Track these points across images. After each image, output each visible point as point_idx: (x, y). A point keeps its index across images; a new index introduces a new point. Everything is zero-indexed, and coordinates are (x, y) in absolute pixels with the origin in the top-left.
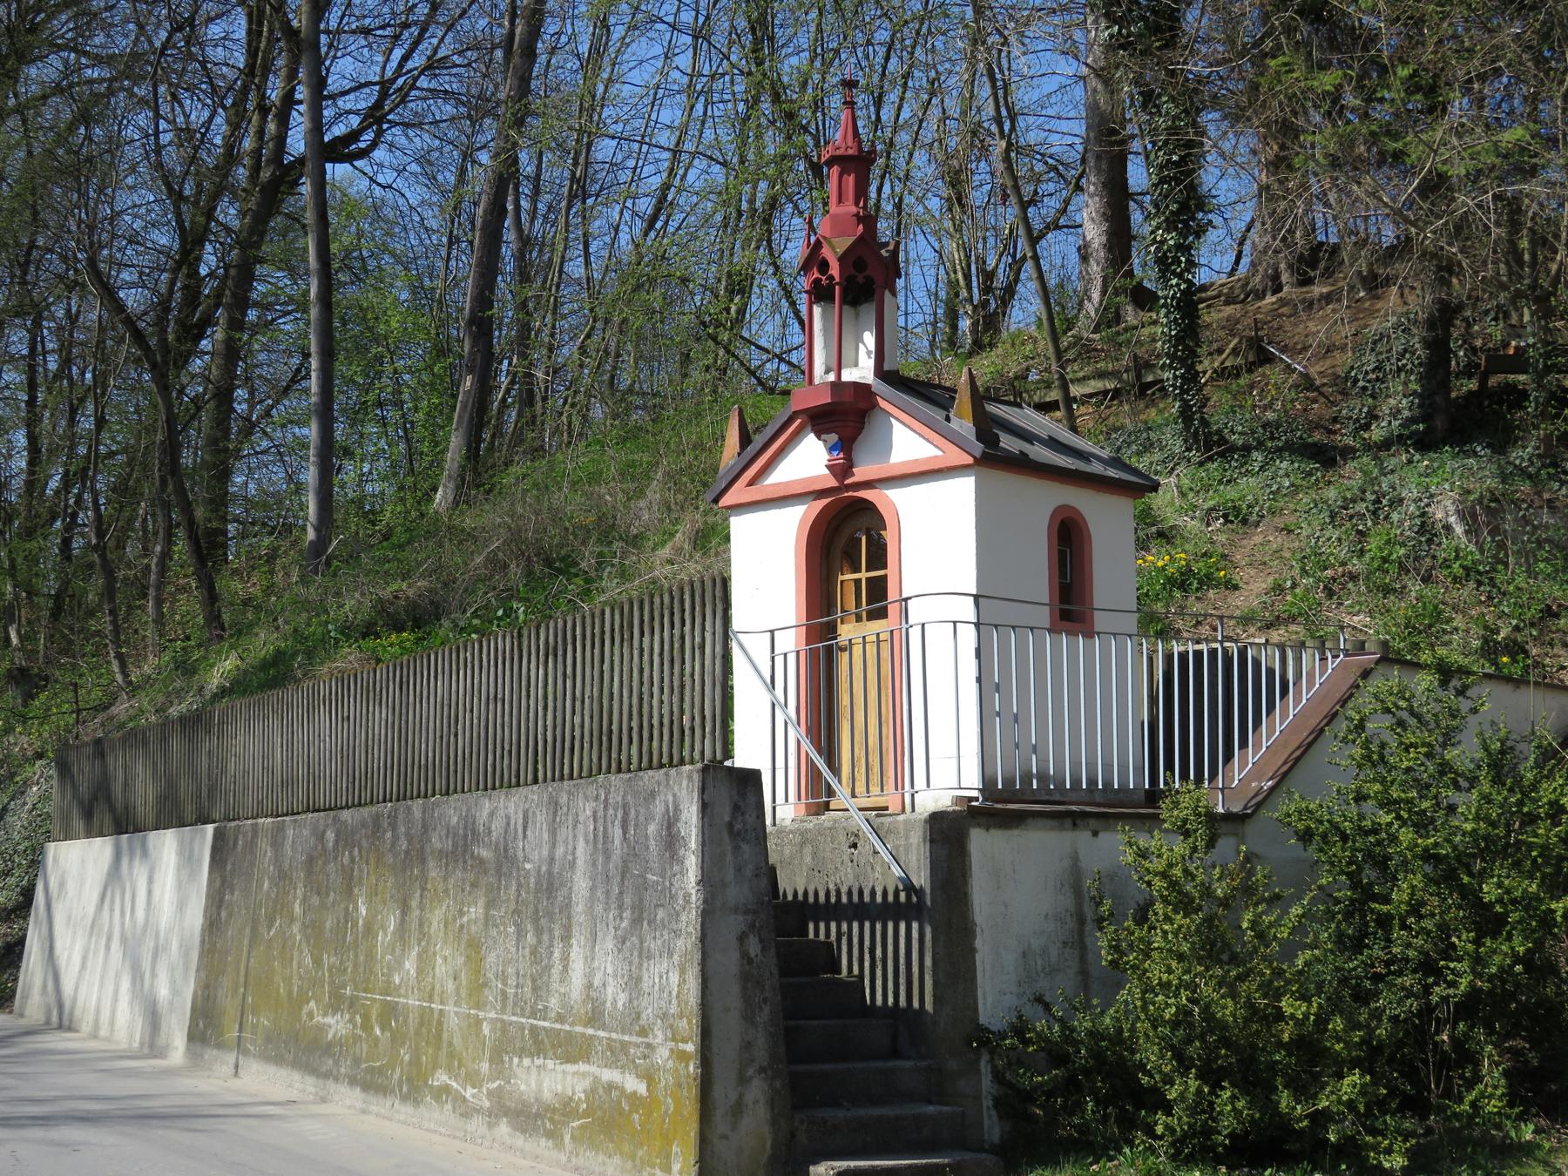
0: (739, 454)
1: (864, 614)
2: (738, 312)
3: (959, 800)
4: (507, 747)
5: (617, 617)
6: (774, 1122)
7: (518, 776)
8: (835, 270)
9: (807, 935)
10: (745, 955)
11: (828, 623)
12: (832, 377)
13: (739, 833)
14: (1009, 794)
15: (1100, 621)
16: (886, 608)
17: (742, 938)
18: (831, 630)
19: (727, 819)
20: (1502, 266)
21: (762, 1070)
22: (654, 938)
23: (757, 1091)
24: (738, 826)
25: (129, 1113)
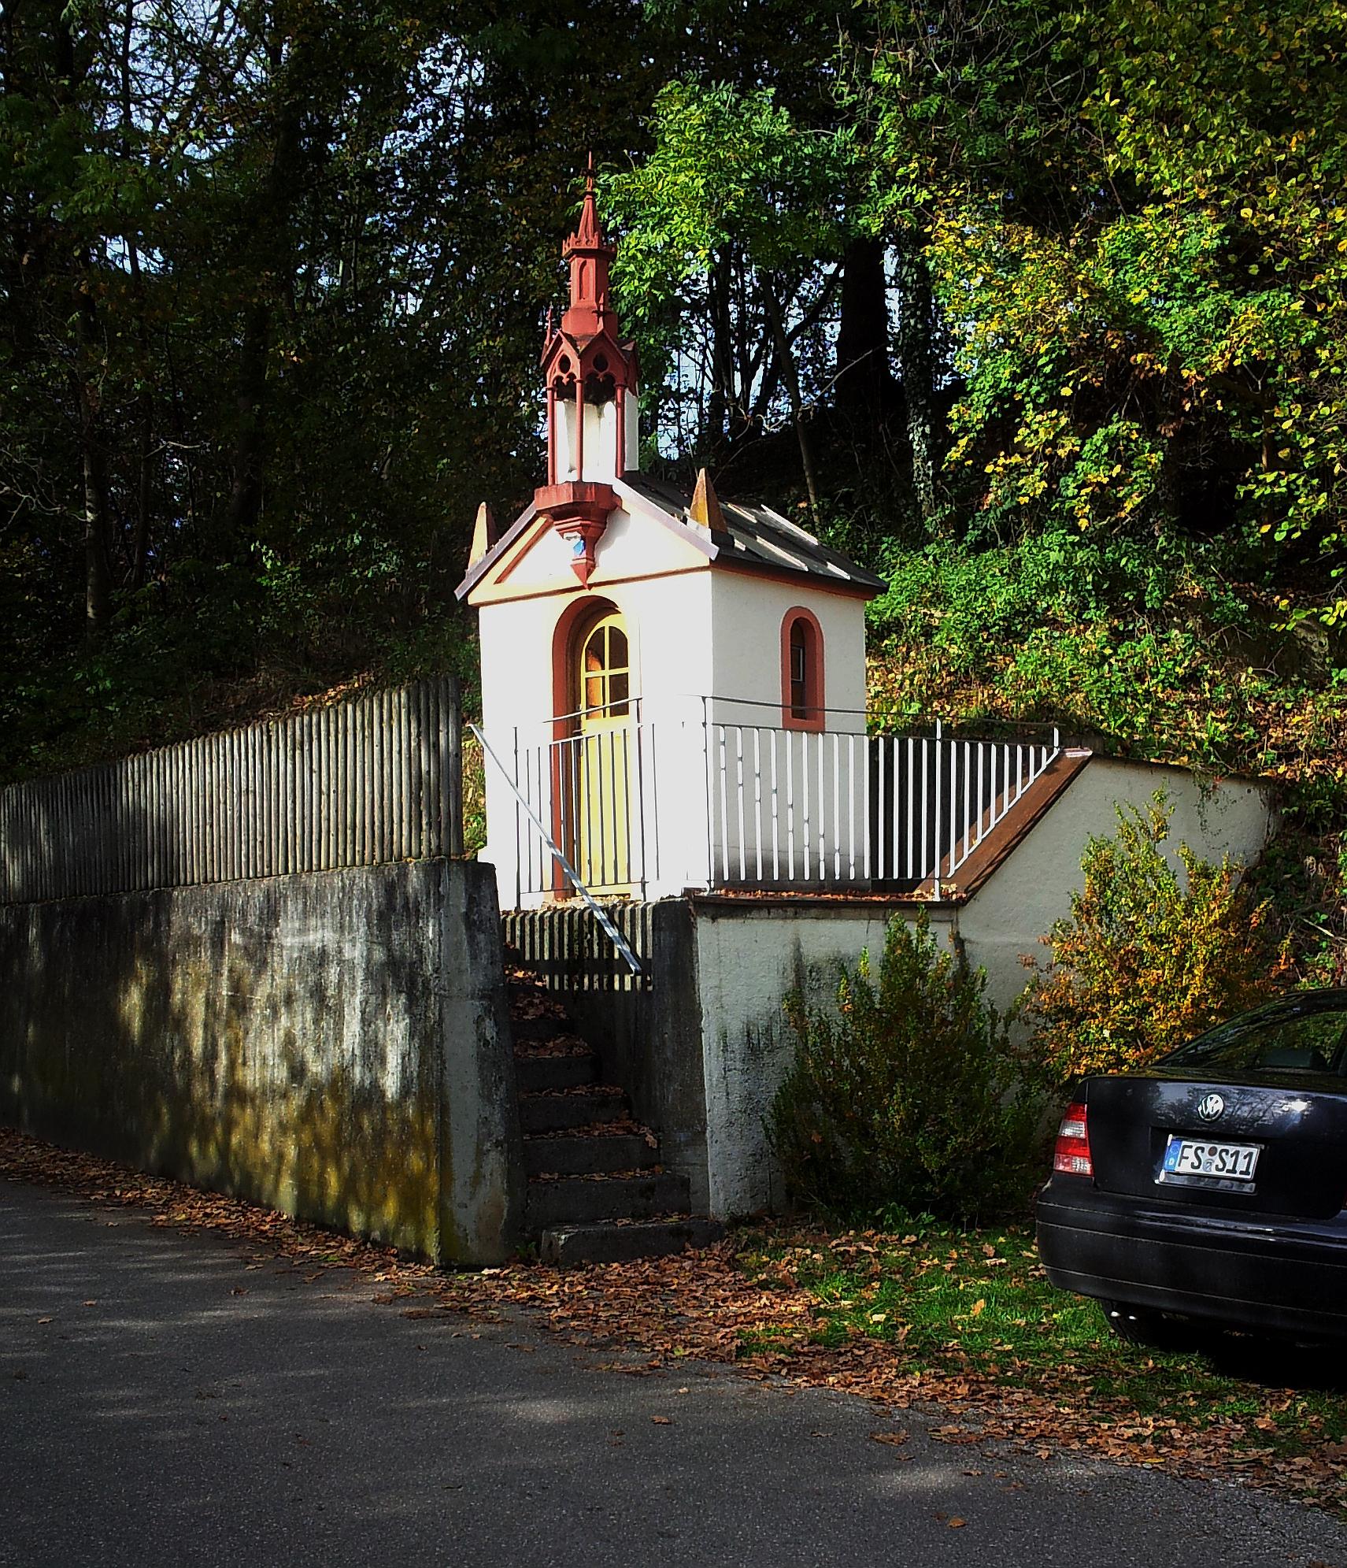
0: (487, 552)
1: (608, 710)
3: (688, 892)
4: (259, 838)
5: (358, 714)
6: (510, 1192)
7: (270, 866)
8: (576, 368)
10: (481, 1037)
11: (623, 704)
12: (574, 477)
14: (734, 884)
15: (831, 720)
16: (627, 704)
17: (479, 1021)
18: (574, 726)
19: (463, 910)
21: (498, 1144)
22: (397, 1021)
23: (494, 1161)
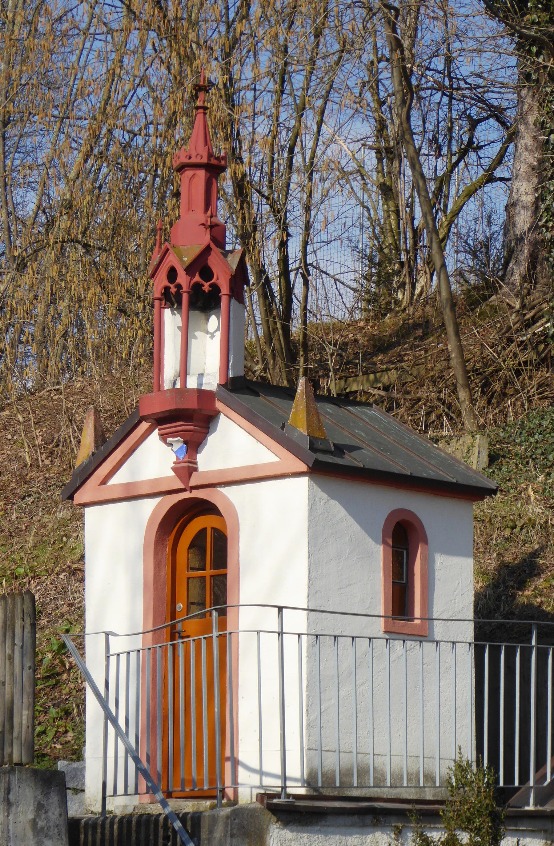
2: (76, 347)
9: (513, 783)
13: (42, 828)
19: (31, 816)
20: (479, 104)
24: (40, 824)
25: (234, 701)
